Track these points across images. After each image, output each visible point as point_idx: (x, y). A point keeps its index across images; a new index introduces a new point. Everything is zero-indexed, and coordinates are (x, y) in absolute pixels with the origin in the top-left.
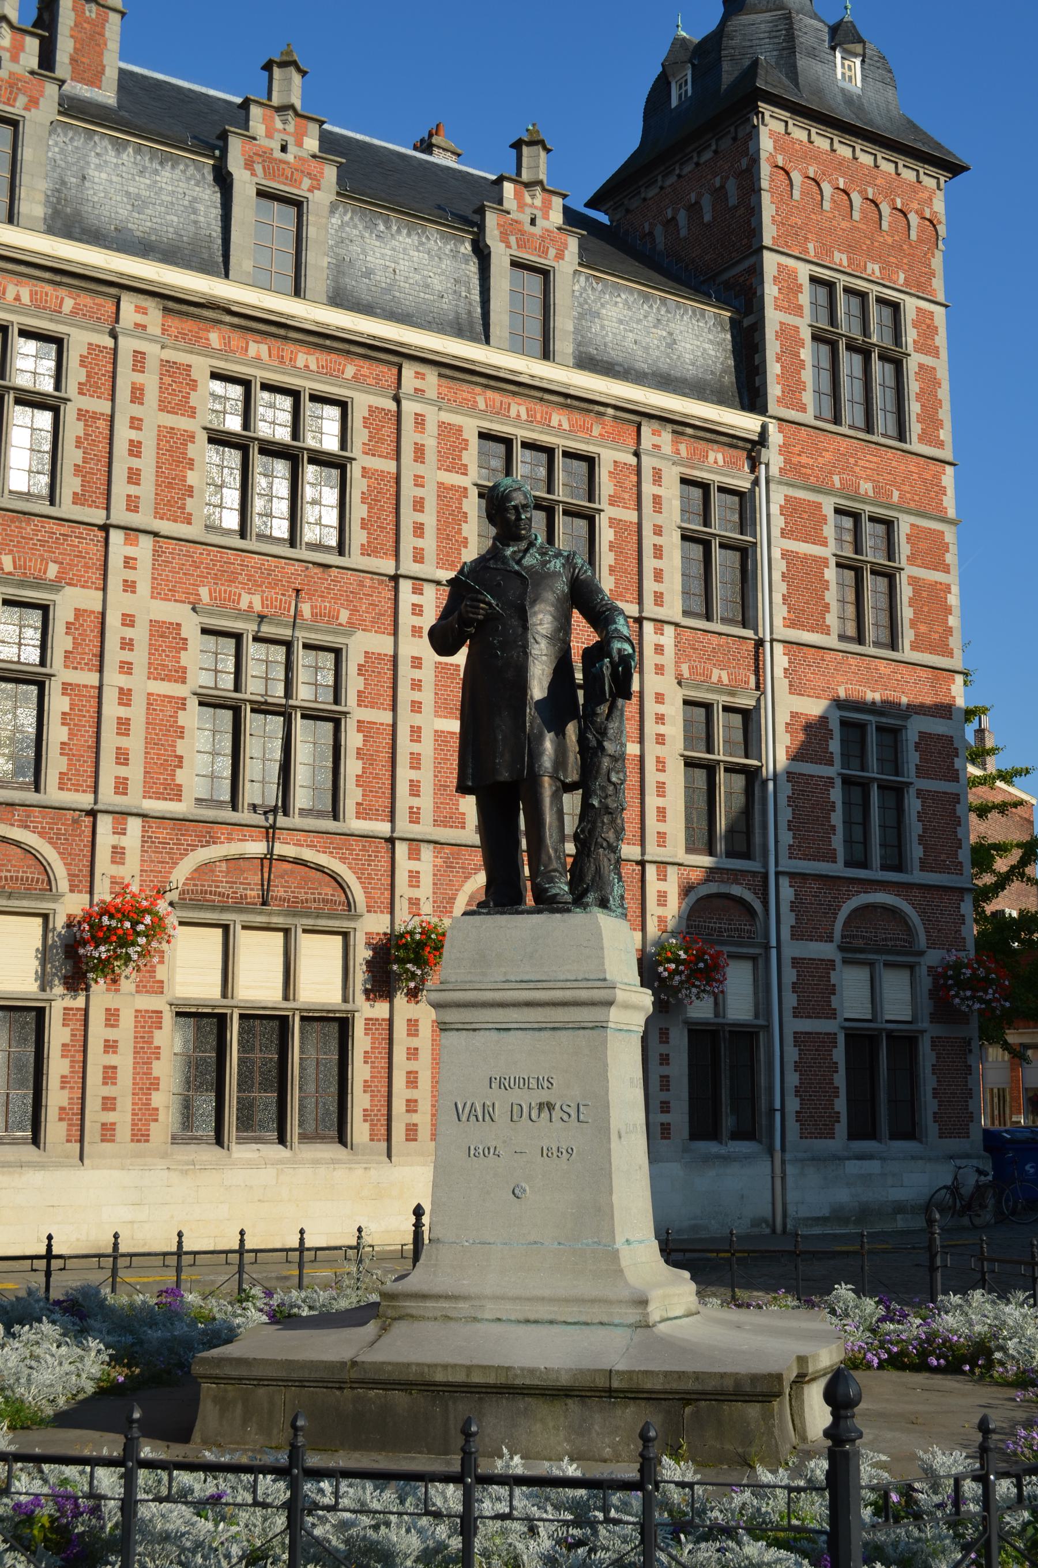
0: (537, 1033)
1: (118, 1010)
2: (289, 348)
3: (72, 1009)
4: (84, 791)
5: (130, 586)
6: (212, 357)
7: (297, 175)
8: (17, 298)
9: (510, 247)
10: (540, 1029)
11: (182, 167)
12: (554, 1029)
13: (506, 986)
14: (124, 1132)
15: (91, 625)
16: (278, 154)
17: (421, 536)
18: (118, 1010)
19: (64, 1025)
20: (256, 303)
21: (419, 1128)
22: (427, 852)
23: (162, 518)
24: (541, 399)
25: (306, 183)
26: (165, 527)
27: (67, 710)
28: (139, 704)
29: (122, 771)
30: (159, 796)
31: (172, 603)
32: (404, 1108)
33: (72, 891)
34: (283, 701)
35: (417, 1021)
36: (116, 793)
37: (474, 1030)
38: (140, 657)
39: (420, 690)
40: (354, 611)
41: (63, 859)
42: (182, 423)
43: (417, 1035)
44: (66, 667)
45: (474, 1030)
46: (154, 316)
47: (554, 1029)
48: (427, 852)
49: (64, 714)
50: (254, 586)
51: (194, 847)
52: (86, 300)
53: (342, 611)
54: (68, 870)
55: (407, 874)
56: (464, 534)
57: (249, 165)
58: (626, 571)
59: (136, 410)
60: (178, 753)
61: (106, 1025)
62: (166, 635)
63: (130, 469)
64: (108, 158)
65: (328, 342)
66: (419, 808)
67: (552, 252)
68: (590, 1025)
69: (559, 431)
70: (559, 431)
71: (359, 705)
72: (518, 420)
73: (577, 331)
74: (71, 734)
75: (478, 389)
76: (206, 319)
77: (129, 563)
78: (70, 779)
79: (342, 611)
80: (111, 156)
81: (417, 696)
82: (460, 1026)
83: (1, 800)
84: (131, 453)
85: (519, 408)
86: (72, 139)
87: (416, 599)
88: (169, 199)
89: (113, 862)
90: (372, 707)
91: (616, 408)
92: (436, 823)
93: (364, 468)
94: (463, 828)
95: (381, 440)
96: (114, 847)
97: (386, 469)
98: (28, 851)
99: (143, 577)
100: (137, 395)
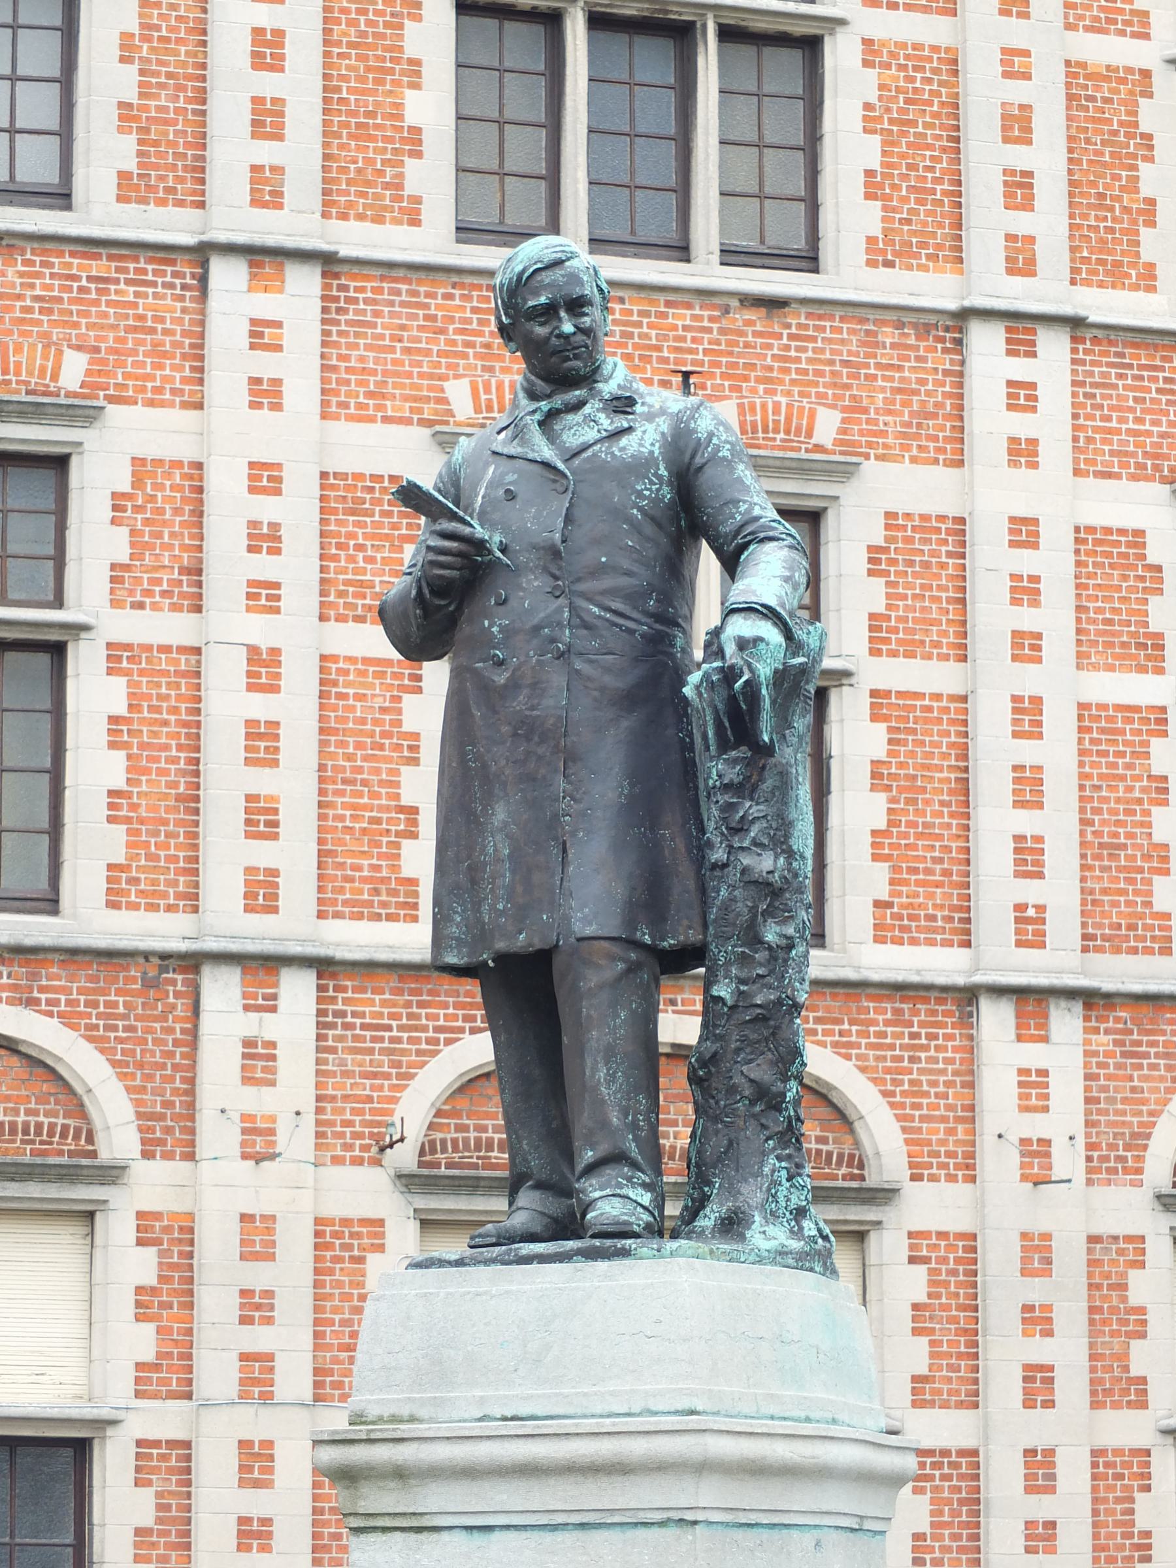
0: (548, 1537)
1: (269, 1444)
3: (156, 1444)
4: (170, 908)
5: (265, 394)
10: (554, 1528)
12: (583, 1526)
15: (168, 494)
17: (1027, 205)
18: (269, 1444)
19: (137, 1483)
22: (1066, 1022)
23: (344, 217)
26: (354, 239)
27: (122, 710)
28: (1060, 723)
29: (263, 854)
30: (359, 911)
31: (379, 426)
33: (147, 1155)
35: (1050, 1452)
36: (248, 909)
38: (1055, 619)
39: (1035, 603)
40: (856, 408)
41: (122, 1077)
43: (1052, 1490)
44: (116, 603)
47: (583, 1526)
49: (113, 720)
53: (70, 356)
54: (138, 1103)
55: (1014, 1078)
56: (1146, 191)
60: (405, 801)
61: (242, 1483)
63: (256, 100)
66: (1041, 908)
68: (658, 1516)
71: (874, 652)
74: (134, 769)
78: (135, 881)
79: (70, 356)
81: (1027, 619)
82: (388, 1522)
83: (3, 938)
84: (259, 62)
87: (1020, 368)
89: (247, 1080)
90: (910, 655)
93: (867, 42)
96: (248, 1043)
98: (40, 1066)
99: (1051, 423)
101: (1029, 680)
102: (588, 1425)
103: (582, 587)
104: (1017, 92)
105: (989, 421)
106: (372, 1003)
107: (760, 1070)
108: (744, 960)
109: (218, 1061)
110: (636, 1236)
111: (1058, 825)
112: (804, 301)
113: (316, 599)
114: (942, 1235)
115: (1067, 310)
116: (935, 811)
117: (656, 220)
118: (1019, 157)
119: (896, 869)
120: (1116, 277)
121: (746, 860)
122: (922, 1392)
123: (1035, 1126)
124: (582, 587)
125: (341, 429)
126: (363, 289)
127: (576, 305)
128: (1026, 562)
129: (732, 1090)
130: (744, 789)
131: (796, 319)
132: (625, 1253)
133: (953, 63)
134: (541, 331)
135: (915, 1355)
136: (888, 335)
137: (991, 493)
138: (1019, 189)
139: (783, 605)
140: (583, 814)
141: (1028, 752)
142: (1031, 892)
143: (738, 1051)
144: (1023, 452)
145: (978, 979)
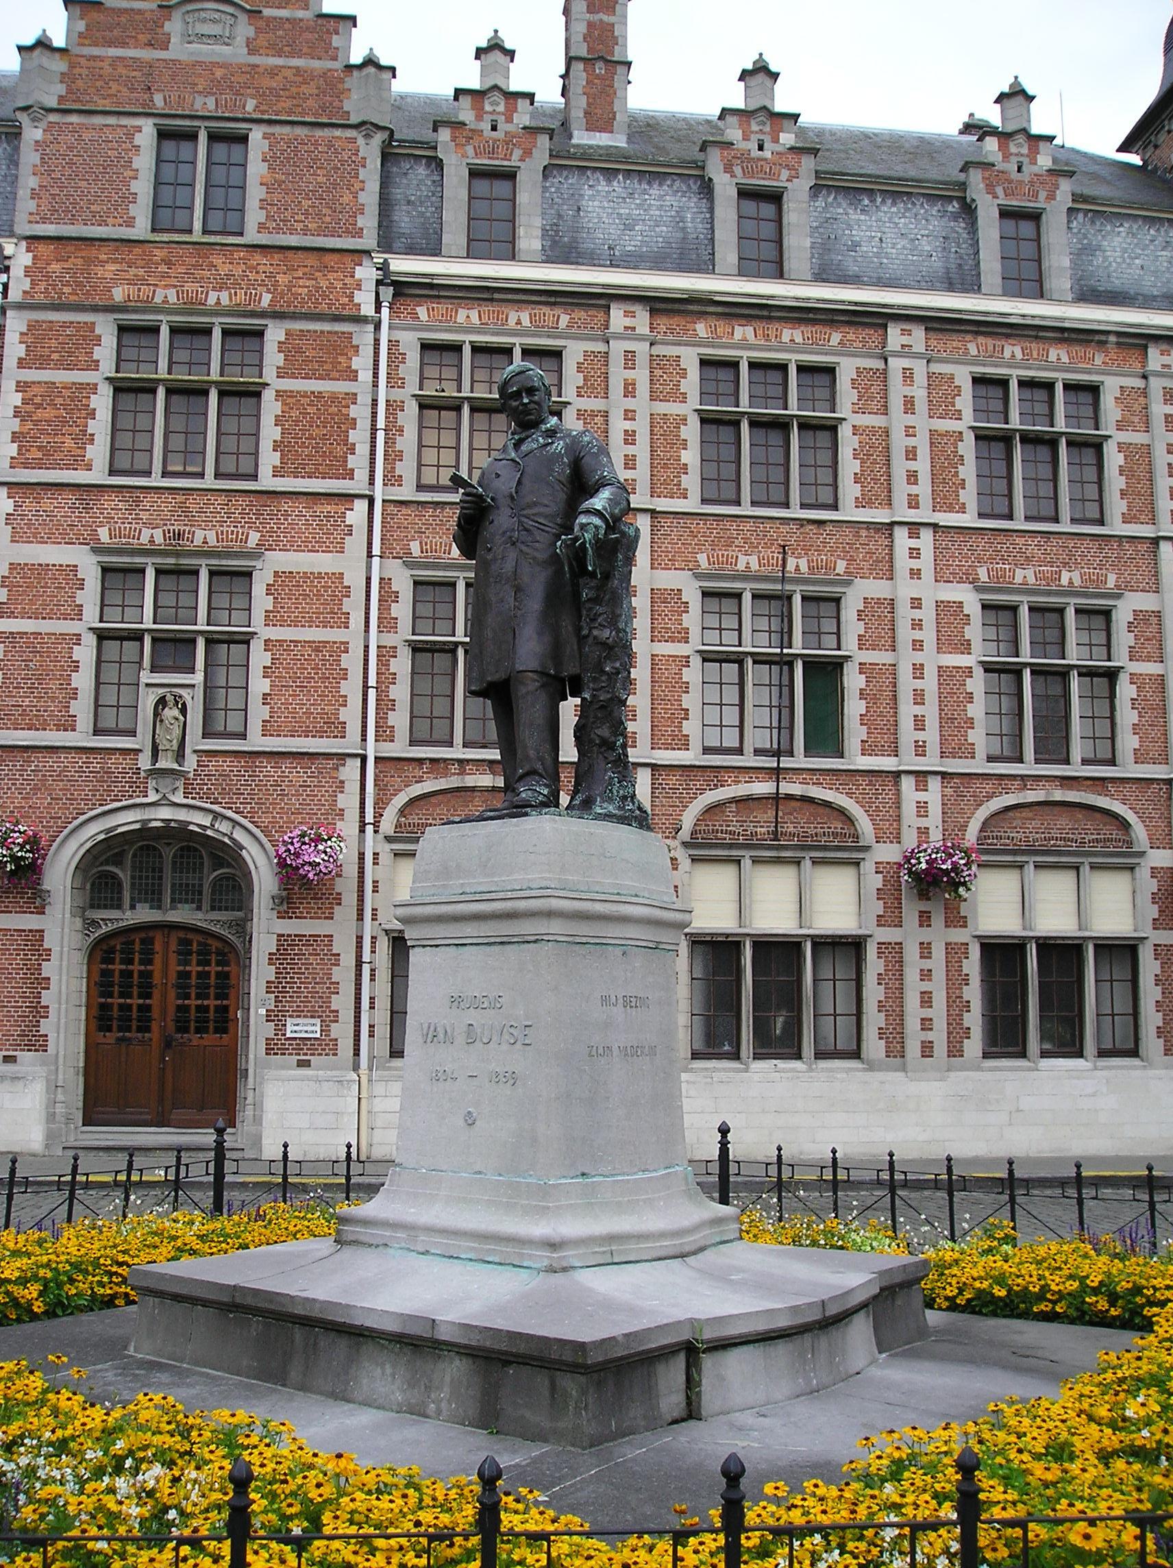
0: (488, 948)
2: (773, 327)
6: (700, 346)
7: (775, 169)
8: (519, 322)
9: (996, 197)
11: (669, 182)
13: (463, 898)
14: (941, 1048)
16: (756, 153)
20: (827, 296)
21: (935, 1045)
24: (1036, 337)
25: (785, 174)
26: (662, 504)
28: (931, 674)
32: (919, 1027)
34: (778, 650)
37: (437, 946)
38: (928, 635)
42: (673, 408)
45: (437, 946)
46: (642, 319)
48: (934, 784)
50: (751, 548)
51: (702, 791)
52: (581, 314)
55: (915, 805)
57: (728, 169)
58: (1139, 494)
59: (910, 420)
62: (949, 612)
64: (600, 188)
65: (1081, 337)
66: (924, 742)
67: (1042, 195)
69: (792, 347)
70: (792, 347)
72: (1013, 360)
73: (1075, 265)
75: (969, 337)
76: (692, 312)
77: (914, 553)
80: (603, 186)
81: (918, 635)
84: (626, 442)
85: (1013, 350)
86: (567, 178)
87: (913, 543)
88: (657, 213)
91: (1118, 334)
92: (943, 755)
94: (973, 757)
95: (872, 398)
97: (877, 425)
99: (926, 562)
100: (630, 389)
101: (919, 657)
102: (501, 895)
103: (525, 512)
104: (912, 442)
105: (903, 562)
106: (673, 779)
107: (604, 732)
108: (595, 680)
109: (909, 809)
110: (532, 806)
111: (931, 711)
112: (831, 521)
113: (649, 634)
114: (888, 863)
115: (932, 521)
116: (884, 706)
117: (776, 494)
118: (912, 465)
119: (869, 728)
120: (951, 509)
121: (595, 632)
122: (881, 921)
123: (923, 822)
124: (525, 512)
125: (659, 573)
126: (666, 522)
127: (531, 391)
128: (917, 614)
129: (591, 741)
130: (596, 600)
131: (829, 528)
132: (526, 814)
133: (887, 432)
134: (515, 404)
135: (879, 908)
136: (864, 533)
137: (905, 589)
138: (912, 477)
139: (605, 509)
140: (523, 615)
141: (919, 684)
142: (921, 736)
143: (594, 723)
144: (915, 574)
145: (901, 768)
